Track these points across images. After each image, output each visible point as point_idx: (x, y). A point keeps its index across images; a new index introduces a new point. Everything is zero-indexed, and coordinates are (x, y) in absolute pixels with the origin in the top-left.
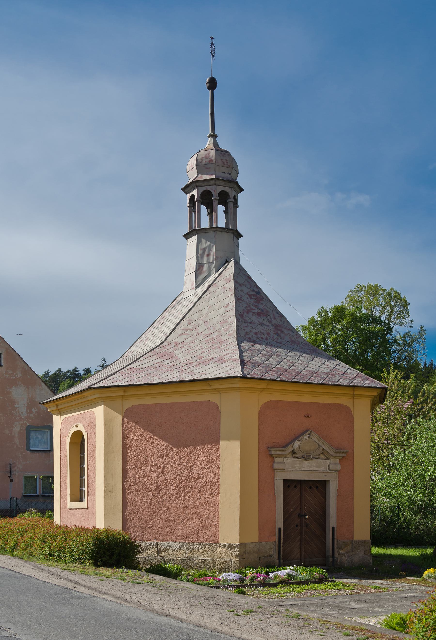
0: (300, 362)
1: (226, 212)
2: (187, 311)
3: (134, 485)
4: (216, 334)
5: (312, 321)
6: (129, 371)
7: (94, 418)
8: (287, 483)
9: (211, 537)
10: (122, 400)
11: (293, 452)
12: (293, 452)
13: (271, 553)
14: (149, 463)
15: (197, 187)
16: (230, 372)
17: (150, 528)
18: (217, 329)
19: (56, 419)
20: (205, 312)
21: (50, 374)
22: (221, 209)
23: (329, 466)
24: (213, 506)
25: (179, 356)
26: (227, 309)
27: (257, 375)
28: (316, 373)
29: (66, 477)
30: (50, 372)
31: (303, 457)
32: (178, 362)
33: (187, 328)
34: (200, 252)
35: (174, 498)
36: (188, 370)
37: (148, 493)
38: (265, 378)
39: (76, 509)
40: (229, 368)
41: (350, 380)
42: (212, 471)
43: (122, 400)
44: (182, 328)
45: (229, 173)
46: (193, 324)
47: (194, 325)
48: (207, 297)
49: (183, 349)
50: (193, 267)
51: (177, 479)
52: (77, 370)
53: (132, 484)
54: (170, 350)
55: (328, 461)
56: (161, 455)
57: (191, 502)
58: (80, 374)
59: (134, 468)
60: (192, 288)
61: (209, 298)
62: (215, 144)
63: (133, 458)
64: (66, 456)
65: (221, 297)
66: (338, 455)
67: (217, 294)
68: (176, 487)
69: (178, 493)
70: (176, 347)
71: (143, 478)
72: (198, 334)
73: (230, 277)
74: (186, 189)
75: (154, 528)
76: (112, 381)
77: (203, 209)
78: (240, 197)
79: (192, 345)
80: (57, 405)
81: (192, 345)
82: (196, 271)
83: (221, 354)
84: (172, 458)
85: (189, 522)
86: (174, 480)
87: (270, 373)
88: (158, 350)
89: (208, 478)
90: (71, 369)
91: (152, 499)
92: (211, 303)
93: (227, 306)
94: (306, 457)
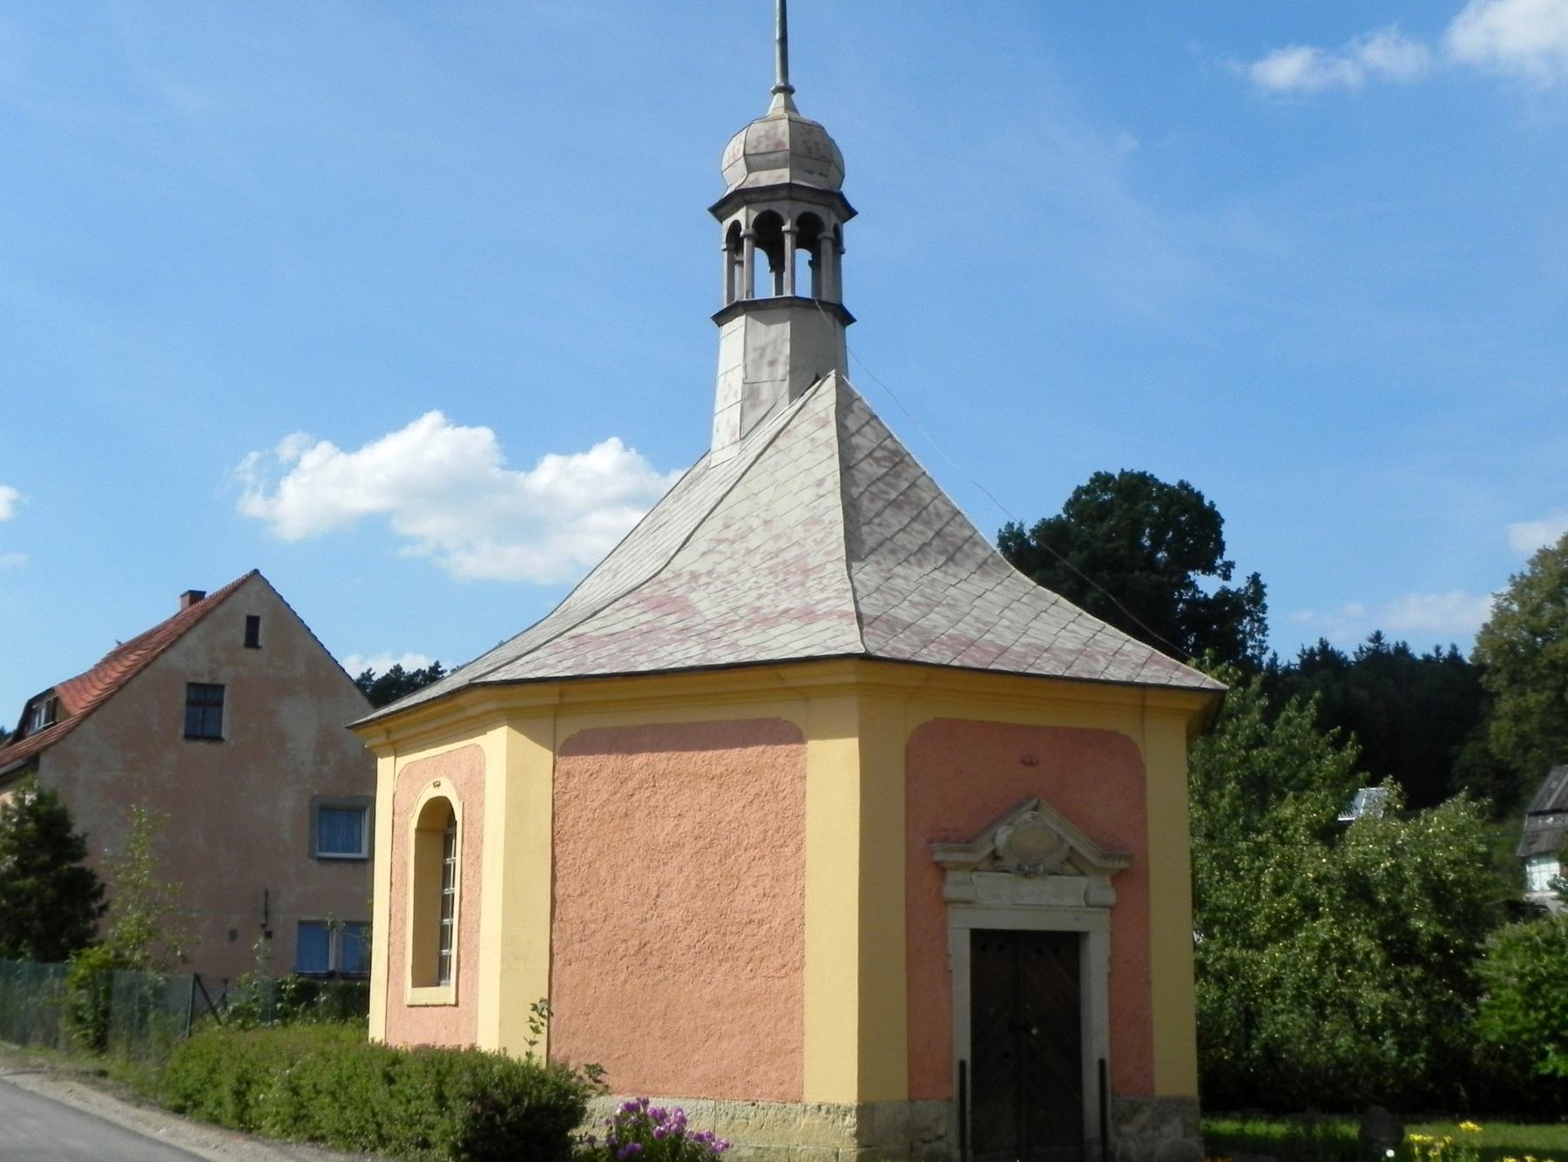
0: (1005, 622)
4: (794, 551)
6: (573, 641)
7: (483, 764)
8: (981, 939)
9: (781, 1084)
10: (555, 716)
11: (995, 856)
12: (995, 856)
13: (941, 1131)
14: (622, 882)
15: (748, 203)
16: (831, 643)
17: (619, 1058)
18: (795, 538)
19: (388, 769)
20: (765, 498)
21: (375, 678)
23: (1086, 895)
24: (787, 1000)
26: (822, 491)
27: (901, 651)
31: (1019, 868)
32: (698, 620)
33: (720, 537)
34: (752, 355)
35: (685, 976)
36: (725, 639)
37: (616, 963)
39: (427, 1006)
40: (829, 634)
41: (1133, 669)
42: (784, 903)
43: (555, 716)
44: (708, 537)
45: (821, 174)
47: (739, 529)
48: (771, 461)
49: (711, 589)
52: (440, 669)
54: (679, 592)
55: (1083, 881)
57: (730, 987)
60: (733, 440)
62: (790, 107)
63: (579, 867)
64: (405, 864)
66: (1109, 864)
67: (794, 454)
68: (689, 947)
70: (693, 585)
72: (749, 552)
73: (828, 415)
74: (721, 209)
75: (630, 1057)
76: (531, 666)
80: (388, 732)
81: (733, 577)
83: (807, 599)
84: (680, 871)
85: (724, 1045)
87: (932, 647)
89: (775, 923)
91: (626, 981)
94: (1027, 871)
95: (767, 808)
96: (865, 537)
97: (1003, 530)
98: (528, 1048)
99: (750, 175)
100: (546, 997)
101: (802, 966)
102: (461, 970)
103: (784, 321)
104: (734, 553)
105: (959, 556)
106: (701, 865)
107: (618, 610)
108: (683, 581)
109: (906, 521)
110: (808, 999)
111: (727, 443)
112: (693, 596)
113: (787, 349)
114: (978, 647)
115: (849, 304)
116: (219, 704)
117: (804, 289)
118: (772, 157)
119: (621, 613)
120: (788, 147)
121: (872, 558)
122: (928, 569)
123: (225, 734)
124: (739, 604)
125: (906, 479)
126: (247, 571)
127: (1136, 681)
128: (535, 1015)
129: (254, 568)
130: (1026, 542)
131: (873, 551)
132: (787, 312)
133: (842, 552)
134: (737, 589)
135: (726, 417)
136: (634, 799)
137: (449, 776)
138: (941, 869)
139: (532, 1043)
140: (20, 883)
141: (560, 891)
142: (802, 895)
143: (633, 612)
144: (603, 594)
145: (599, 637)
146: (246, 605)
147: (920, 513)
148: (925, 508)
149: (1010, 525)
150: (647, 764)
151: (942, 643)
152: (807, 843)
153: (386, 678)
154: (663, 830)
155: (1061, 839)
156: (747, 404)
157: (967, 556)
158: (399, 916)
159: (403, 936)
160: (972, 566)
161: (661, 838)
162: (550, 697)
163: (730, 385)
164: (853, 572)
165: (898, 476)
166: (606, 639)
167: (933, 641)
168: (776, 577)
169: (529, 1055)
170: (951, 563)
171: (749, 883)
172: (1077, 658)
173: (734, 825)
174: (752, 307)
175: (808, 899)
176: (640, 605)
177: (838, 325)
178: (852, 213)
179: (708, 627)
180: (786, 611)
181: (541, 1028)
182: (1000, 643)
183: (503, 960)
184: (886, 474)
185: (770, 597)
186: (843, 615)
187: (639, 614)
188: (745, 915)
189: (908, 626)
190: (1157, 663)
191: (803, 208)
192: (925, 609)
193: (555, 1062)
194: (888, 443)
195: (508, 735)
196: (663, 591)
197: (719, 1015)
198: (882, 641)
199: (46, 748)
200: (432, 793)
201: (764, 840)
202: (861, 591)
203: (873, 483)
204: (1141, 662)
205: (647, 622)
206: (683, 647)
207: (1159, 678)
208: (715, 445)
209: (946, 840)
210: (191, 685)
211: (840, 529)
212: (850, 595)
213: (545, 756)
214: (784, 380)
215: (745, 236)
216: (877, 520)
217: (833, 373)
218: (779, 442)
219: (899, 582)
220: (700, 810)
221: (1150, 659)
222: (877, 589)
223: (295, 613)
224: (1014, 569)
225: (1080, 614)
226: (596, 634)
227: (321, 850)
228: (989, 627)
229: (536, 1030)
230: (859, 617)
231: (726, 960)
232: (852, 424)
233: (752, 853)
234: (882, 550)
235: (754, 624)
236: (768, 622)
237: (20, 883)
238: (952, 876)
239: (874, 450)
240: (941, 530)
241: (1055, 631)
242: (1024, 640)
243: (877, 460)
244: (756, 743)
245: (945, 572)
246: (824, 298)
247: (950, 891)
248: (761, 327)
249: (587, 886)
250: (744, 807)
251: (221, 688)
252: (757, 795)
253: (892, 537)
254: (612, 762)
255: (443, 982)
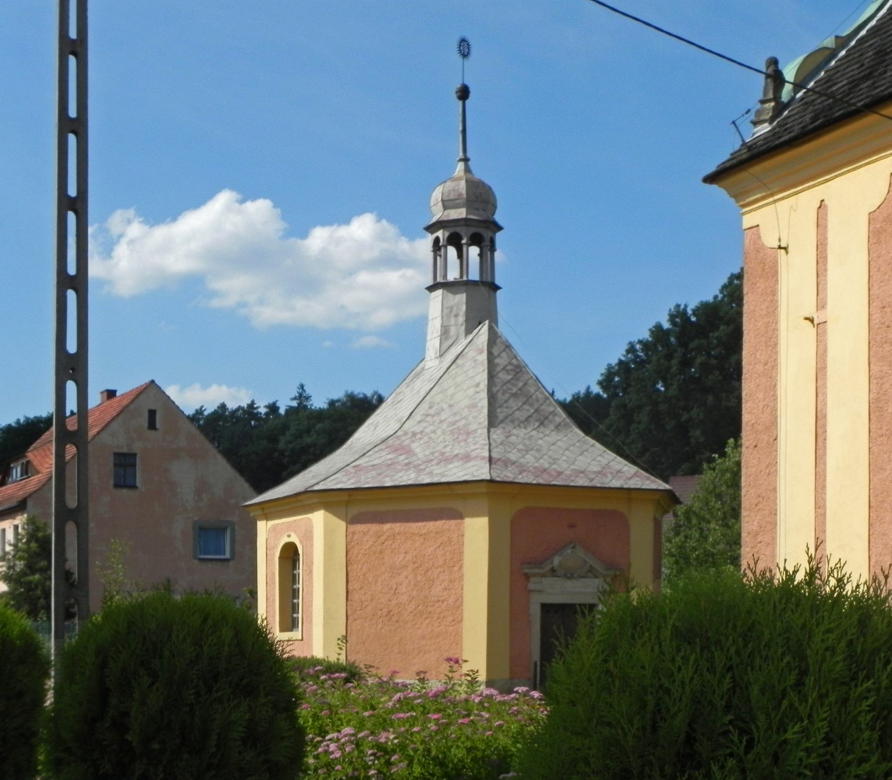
0: (564, 458)
1: (481, 255)
2: (428, 389)
3: (360, 610)
4: (463, 422)
5: (658, 331)
7: (312, 527)
8: (546, 608)
11: (553, 570)
12: (553, 570)
14: (379, 583)
16: (476, 474)
17: (379, 662)
18: (464, 415)
19: (263, 527)
20: (451, 391)
21: (206, 413)
22: (474, 252)
24: (454, 636)
25: (417, 450)
26: (478, 390)
27: (508, 477)
28: (582, 472)
29: (274, 601)
30: (205, 410)
32: (415, 458)
33: (427, 413)
34: (446, 311)
35: (409, 625)
36: (427, 470)
38: (517, 481)
40: (475, 468)
41: (625, 480)
42: (454, 592)
44: (422, 413)
46: (435, 408)
48: (454, 372)
49: (422, 441)
50: (438, 331)
51: (413, 602)
52: (255, 406)
53: (358, 608)
54: (406, 443)
56: (393, 573)
58: (261, 414)
59: (360, 589)
60: (436, 356)
61: (456, 374)
62: (467, 170)
64: (273, 574)
65: (470, 373)
68: (411, 613)
69: (413, 620)
70: (413, 439)
71: (372, 601)
72: (441, 422)
73: (483, 346)
74: (431, 228)
76: (334, 482)
77: (452, 251)
78: (499, 237)
79: (433, 435)
80: (263, 509)
81: (433, 435)
82: (441, 335)
83: (467, 449)
85: (427, 656)
86: (409, 604)
87: (524, 474)
88: (391, 441)
89: (450, 601)
90: (244, 404)
91: (382, 628)
92: (459, 379)
93: (477, 385)
94: (569, 575)
95: (446, 549)
96: (498, 415)
97: (672, 310)
98: (337, 656)
99: (445, 212)
100: (345, 634)
101: (462, 620)
102: (304, 624)
103: (462, 293)
104: (434, 422)
105: (546, 422)
106: (416, 575)
107: (377, 452)
108: (407, 437)
109: (520, 404)
110: (465, 635)
111: (433, 357)
112: (413, 445)
113: (464, 308)
114: (547, 473)
115: (498, 282)
116: (134, 465)
117: (474, 274)
118: (457, 202)
119: (378, 453)
120: (465, 196)
121: (502, 425)
122: (529, 429)
123: (138, 484)
124: (435, 450)
125: (522, 381)
126: (147, 380)
127: (625, 487)
128: (340, 642)
129: (151, 379)
130: (689, 318)
131: (502, 422)
132: (464, 288)
133: (486, 423)
134: (435, 442)
135: (433, 343)
136: (385, 545)
137: (295, 532)
138: (527, 577)
139: (339, 654)
140: (31, 578)
141: (350, 588)
142: (462, 589)
143: (383, 453)
144: (369, 439)
145: (368, 467)
146: (148, 403)
147: (528, 399)
148: (531, 397)
149: (678, 306)
150: (390, 529)
151: (529, 471)
152: (465, 565)
153: (215, 413)
154: (398, 559)
155: (586, 562)
156: (444, 337)
157: (551, 422)
158: (271, 599)
159: (274, 608)
160: (552, 427)
161: (397, 562)
162: (344, 497)
163: (434, 326)
164: (491, 434)
165: (518, 379)
166: (370, 468)
167: (525, 471)
168: (454, 436)
169: (338, 659)
170: (541, 426)
171: (438, 583)
172: (597, 476)
173: (431, 557)
174: (447, 286)
175: (465, 591)
176: (386, 450)
177: (492, 292)
178: (500, 228)
179: (419, 462)
180: (457, 455)
181: (343, 648)
182: (559, 469)
183: (324, 619)
184: (512, 379)
185: (450, 447)
186: (483, 458)
187: (387, 454)
188: (436, 598)
189: (513, 463)
190: (638, 476)
191: (472, 230)
192: (524, 452)
193: (350, 661)
194: (514, 361)
195: (324, 514)
196: (398, 442)
197: (424, 642)
198: (499, 472)
199: (30, 495)
200: (286, 540)
201: (445, 564)
202: (493, 444)
203: (505, 384)
204: (629, 476)
205: (390, 459)
206: (407, 473)
207: (637, 484)
208: (427, 358)
209: (529, 563)
210: (117, 455)
211: (485, 411)
212: (487, 447)
213: (343, 524)
214: (462, 325)
215: (442, 246)
216: (505, 405)
217: (487, 322)
218: (459, 362)
219: (513, 439)
220: (415, 550)
221: (635, 475)
222: (502, 443)
223: (169, 397)
224: (574, 427)
225: (605, 451)
226: (365, 465)
227: (200, 554)
228: (555, 461)
229: (341, 649)
230: (490, 459)
231: (427, 618)
232: (495, 351)
233: (439, 569)
234: (507, 421)
235: (441, 461)
236: (448, 460)
237: (31, 578)
238: (533, 579)
239: (506, 366)
240: (538, 408)
241: (589, 461)
242: (572, 467)
243: (508, 372)
244: (441, 519)
245: (538, 431)
246: (484, 280)
247: (531, 586)
248: (450, 296)
249: (363, 585)
250: (436, 549)
251: (135, 455)
252: (442, 543)
253: (512, 413)
254: (374, 528)
255: (294, 629)
